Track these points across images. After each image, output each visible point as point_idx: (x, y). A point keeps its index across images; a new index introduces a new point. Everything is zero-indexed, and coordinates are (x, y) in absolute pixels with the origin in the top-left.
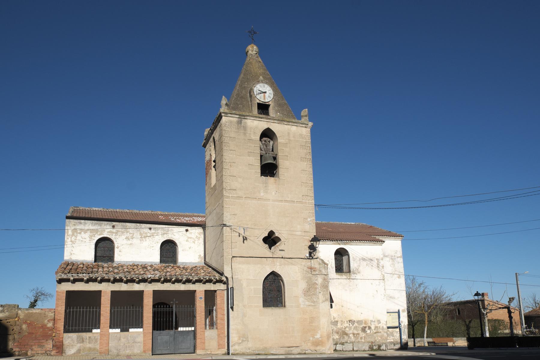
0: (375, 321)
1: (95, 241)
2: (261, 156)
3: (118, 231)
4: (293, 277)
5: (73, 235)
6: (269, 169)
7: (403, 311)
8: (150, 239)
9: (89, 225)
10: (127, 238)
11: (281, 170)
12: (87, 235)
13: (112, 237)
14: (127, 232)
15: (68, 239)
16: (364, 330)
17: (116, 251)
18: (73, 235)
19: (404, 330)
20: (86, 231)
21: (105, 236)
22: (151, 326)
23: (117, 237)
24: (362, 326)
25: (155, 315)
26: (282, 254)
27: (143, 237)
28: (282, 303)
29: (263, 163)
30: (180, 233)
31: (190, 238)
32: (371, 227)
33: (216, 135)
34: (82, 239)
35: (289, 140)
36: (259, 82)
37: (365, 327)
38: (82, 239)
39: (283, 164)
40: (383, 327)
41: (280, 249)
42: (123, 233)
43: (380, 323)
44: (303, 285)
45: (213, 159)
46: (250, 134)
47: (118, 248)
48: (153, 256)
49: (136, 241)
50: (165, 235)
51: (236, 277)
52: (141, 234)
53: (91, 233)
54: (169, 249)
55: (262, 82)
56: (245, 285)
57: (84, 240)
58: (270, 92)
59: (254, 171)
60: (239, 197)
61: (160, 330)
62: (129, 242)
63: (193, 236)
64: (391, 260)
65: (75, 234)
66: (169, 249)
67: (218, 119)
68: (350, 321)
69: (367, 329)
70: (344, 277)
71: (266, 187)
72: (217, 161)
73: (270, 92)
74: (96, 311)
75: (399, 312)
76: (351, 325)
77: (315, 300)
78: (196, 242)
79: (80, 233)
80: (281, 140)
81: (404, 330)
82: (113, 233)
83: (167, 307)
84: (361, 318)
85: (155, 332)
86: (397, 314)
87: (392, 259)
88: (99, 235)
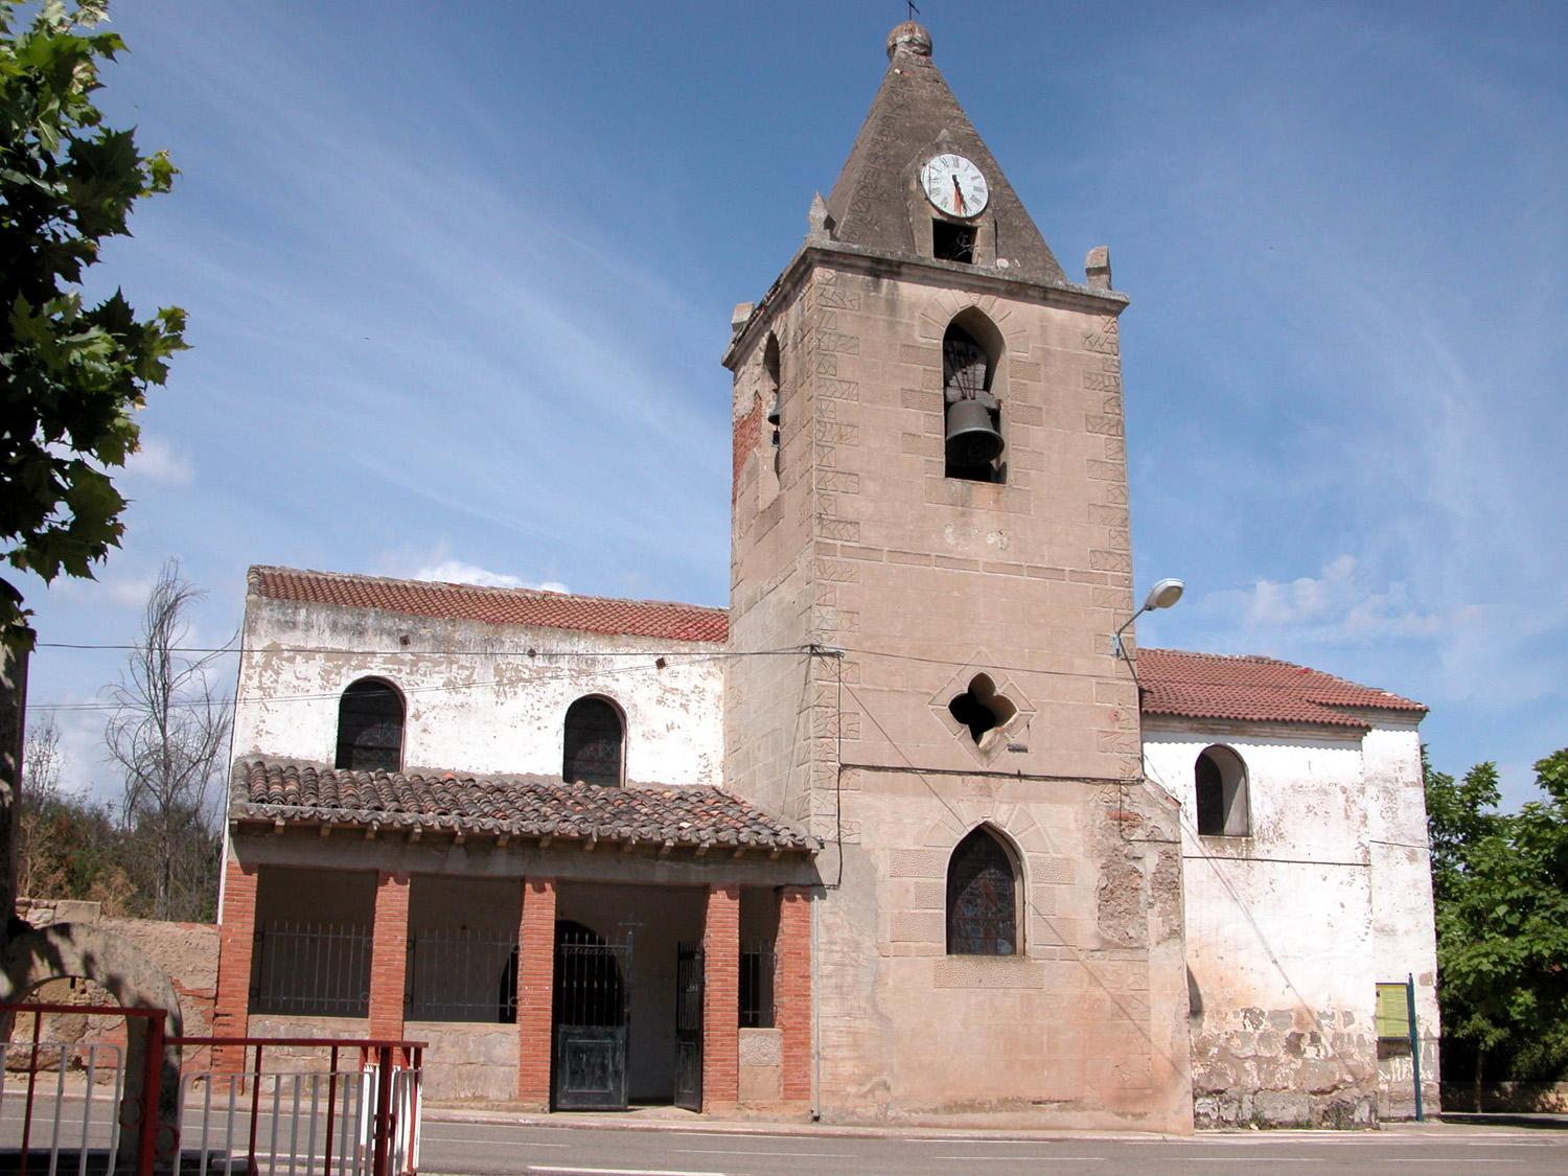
0: (1332, 1016)
1: (341, 690)
2: (948, 405)
3: (418, 657)
4: (1055, 839)
5: (267, 665)
6: (974, 457)
7: (1425, 980)
8: (530, 689)
9: (318, 630)
10: (450, 685)
11: (1013, 457)
12: (313, 668)
13: (401, 679)
14: (452, 663)
15: (250, 678)
16: (1294, 1046)
17: (411, 728)
18: (267, 665)
19: (1428, 1051)
20: (308, 654)
21: (375, 673)
22: (550, 1007)
23: (417, 678)
24: (1288, 1032)
25: (565, 967)
26: (1016, 762)
27: (507, 682)
28: (1013, 941)
29: (948, 437)
30: (638, 675)
31: (673, 691)
32: (1307, 671)
33: (784, 326)
34: (295, 682)
35: (1047, 353)
36: (937, 149)
37: (1300, 1036)
38: (295, 682)
39: (1020, 444)
40: (1361, 1037)
41: (1013, 742)
42: (437, 664)
43: (1352, 1021)
44: (1090, 875)
45: (768, 411)
46: (910, 326)
47: (417, 717)
48: (541, 754)
49: (481, 697)
50: (583, 680)
51: (853, 839)
52: (498, 671)
53: (327, 660)
54: (595, 728)
55: (951, 151)
56: (884, 869)
57: (303, 684)
58: (976, 183)
59: (922, 458)
60: (870, 551)
61: (589, 1023)
62: (459, 698)
63: (681, 683)
64: (1381, 795)
65: (275, 661)
66: (595, 728)
67: (795, 268)
68: (1247, 1011)
69: (1305, 1043)
70: (1230, 851)
71: (963, 514)
72: (787, 418)
73: (976, 183)
74: (358, 943)
75: (1410, 988)
76: (1250, 1029)
77: (1132, 933)
78: (693, 706)
79: (291, 660)
80: (1013, 353)
81: (1428, 1051)
82: (402, 662)
83: (582, 941)
84: (1288, 1001)
85: (563, 1028)
86: (1404, 990)
87: (1386, 790)
88: (358, 668)
